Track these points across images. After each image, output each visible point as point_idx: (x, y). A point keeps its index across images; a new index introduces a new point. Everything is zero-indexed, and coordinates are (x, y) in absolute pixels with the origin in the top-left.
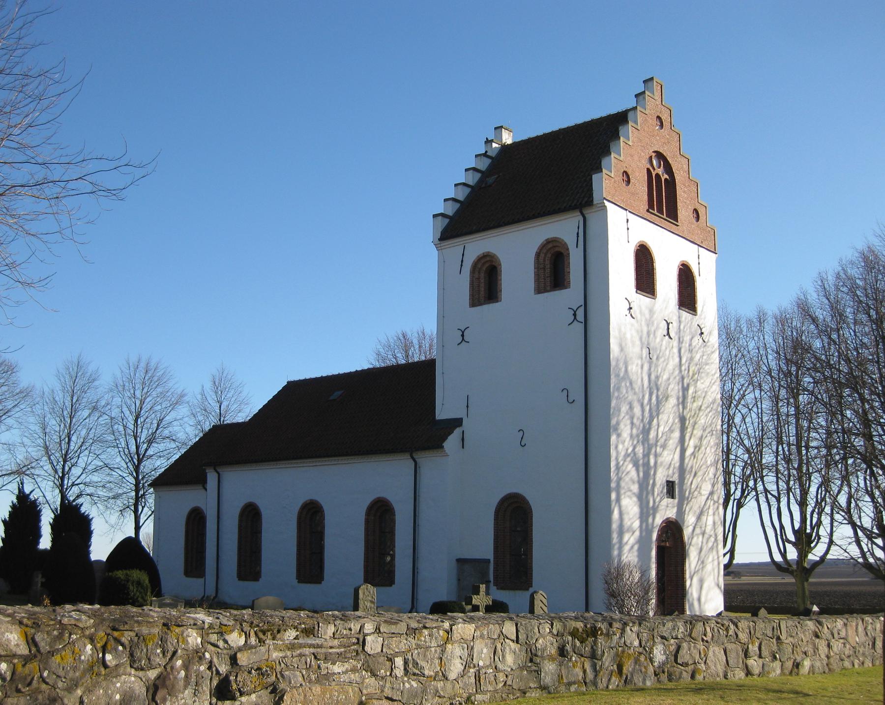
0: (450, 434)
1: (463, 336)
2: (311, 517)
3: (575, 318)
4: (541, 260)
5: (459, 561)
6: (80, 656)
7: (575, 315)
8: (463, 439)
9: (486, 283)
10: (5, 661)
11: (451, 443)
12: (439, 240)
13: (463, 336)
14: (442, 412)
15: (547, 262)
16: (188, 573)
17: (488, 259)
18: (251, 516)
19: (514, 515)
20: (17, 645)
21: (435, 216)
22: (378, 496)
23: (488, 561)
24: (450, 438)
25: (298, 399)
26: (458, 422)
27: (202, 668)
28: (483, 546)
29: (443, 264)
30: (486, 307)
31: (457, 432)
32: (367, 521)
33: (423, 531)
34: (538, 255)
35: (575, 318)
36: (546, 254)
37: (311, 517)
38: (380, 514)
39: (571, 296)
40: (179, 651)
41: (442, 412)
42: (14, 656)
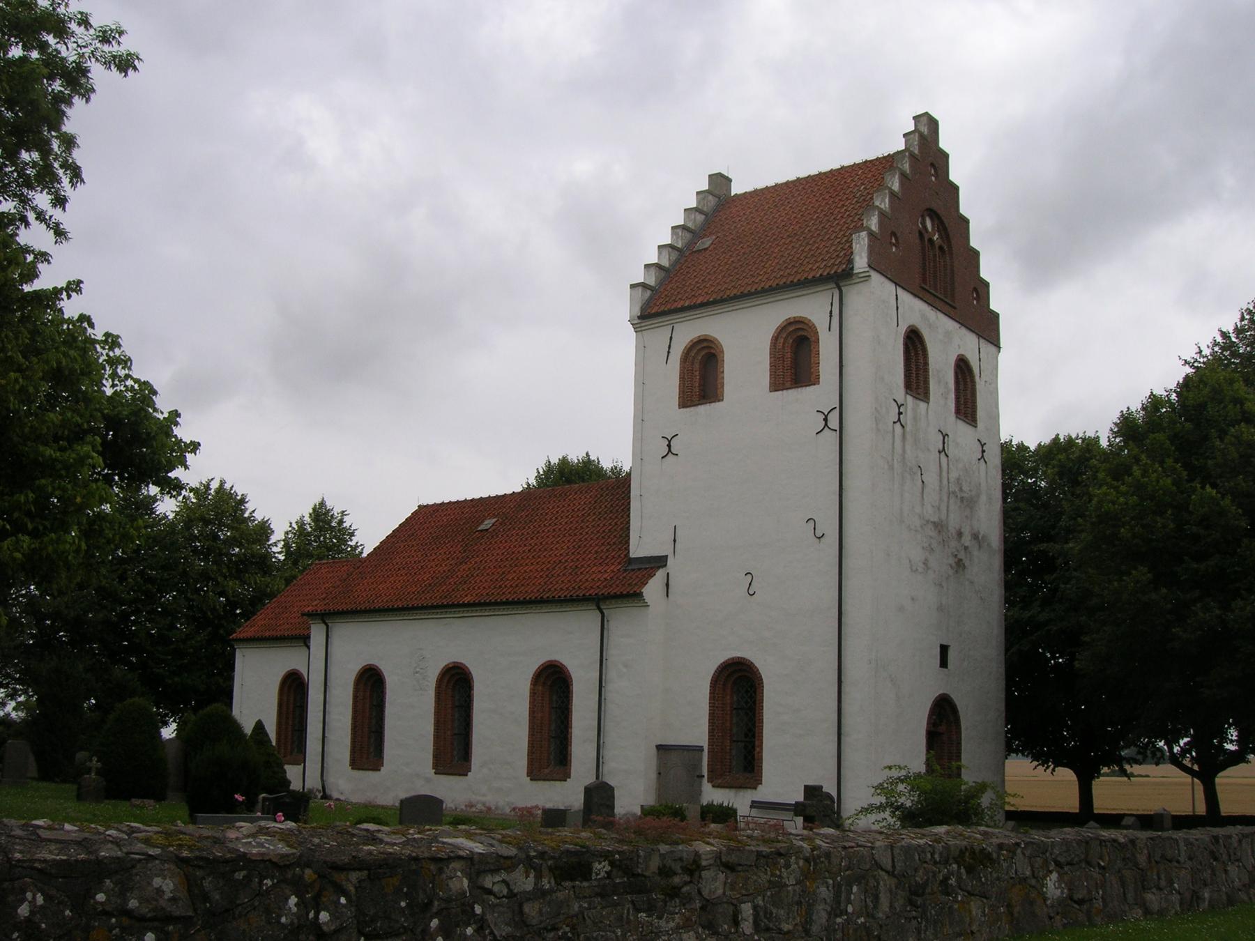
0: (651, 576)
1: (669, 446)
2: (456, 686)
3: (826, 424)
4: (780, 345)
5: (660, 748)
6: (279, 916)
7: (826, 420)
8: (667, 585)
9: (701, 377)
10: (151, 930)
11: (652, 589)
12: (639, 318)
13: (669, 446)
14: (640, 547)
15: (788, 350)
16: (753, 802)
17: (705, 344)
18: (371, 683)
19: (738, 688)
20: (173, 900)
21: (632, 286)
22: (552, 658)
23: (701, 749)
24: (651, 582)
25: (436, 527)
26: (660, 562)
27: (469, 931)
28: (693, 726)
29: (641, 349)
30: (702, 409)
31: (660, 575)
32: (533, 694)
33: (611, 709)
34: (775, 339)
35: (826, 424)
36: (786, 339)
37: (456, 686)
38: (552, 684)
39: (821, 395)
40: (436, 903)
41: (640, 547)
42: (170, 919)
